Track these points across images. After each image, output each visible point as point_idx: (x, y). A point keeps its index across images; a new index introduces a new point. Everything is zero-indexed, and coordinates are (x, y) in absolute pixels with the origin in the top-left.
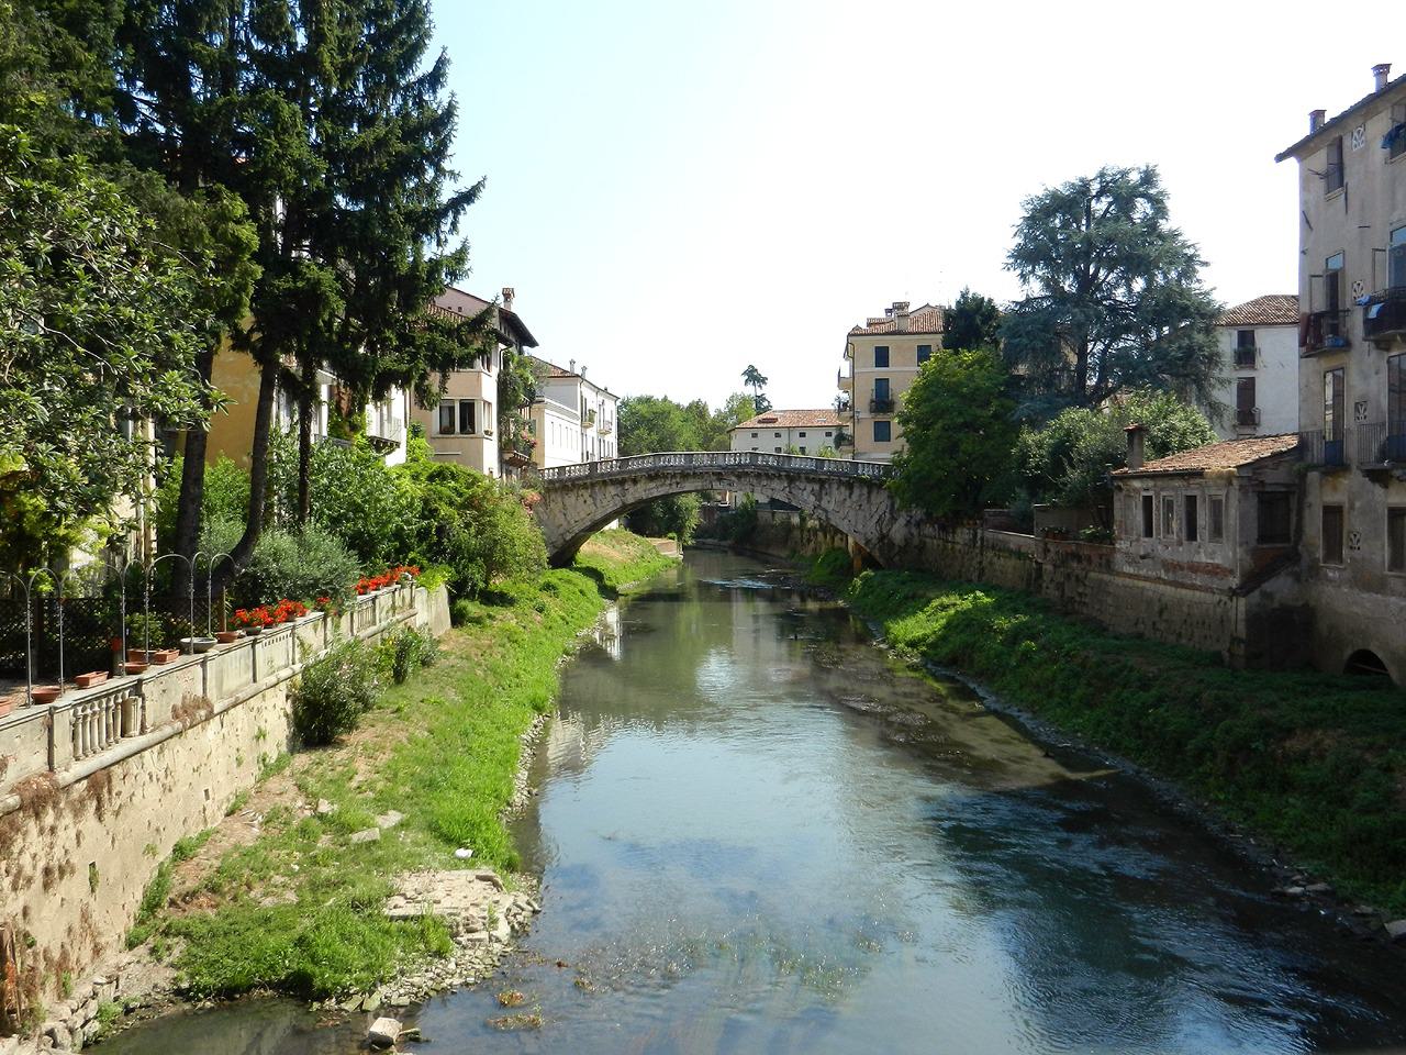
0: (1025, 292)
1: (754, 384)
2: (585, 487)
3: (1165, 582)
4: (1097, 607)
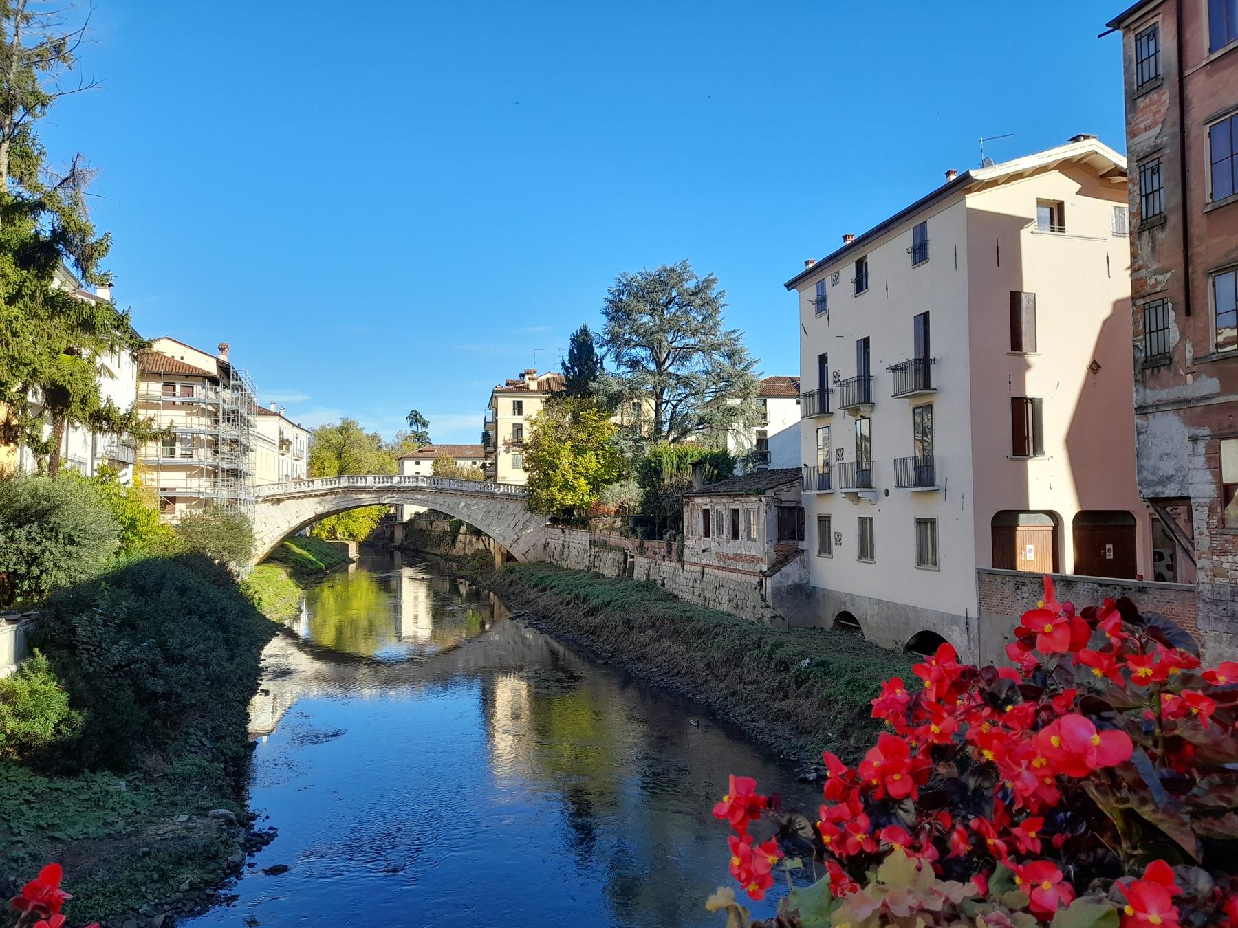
3: (718, 568)
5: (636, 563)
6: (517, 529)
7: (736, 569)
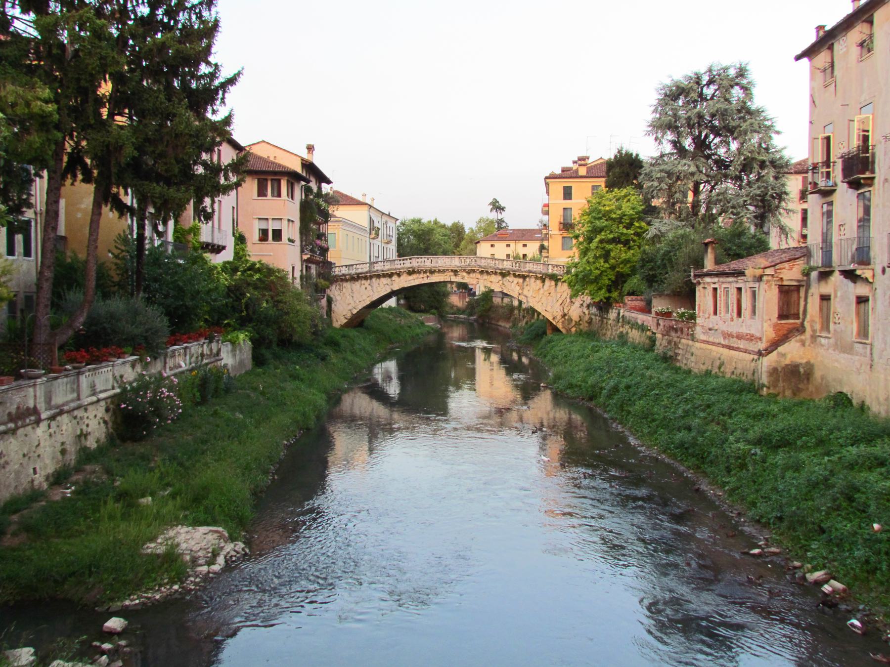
0: (660, 150)
1: (497, 211)
2: (366, 278)
3: (724, 346)
4: (685, 362)
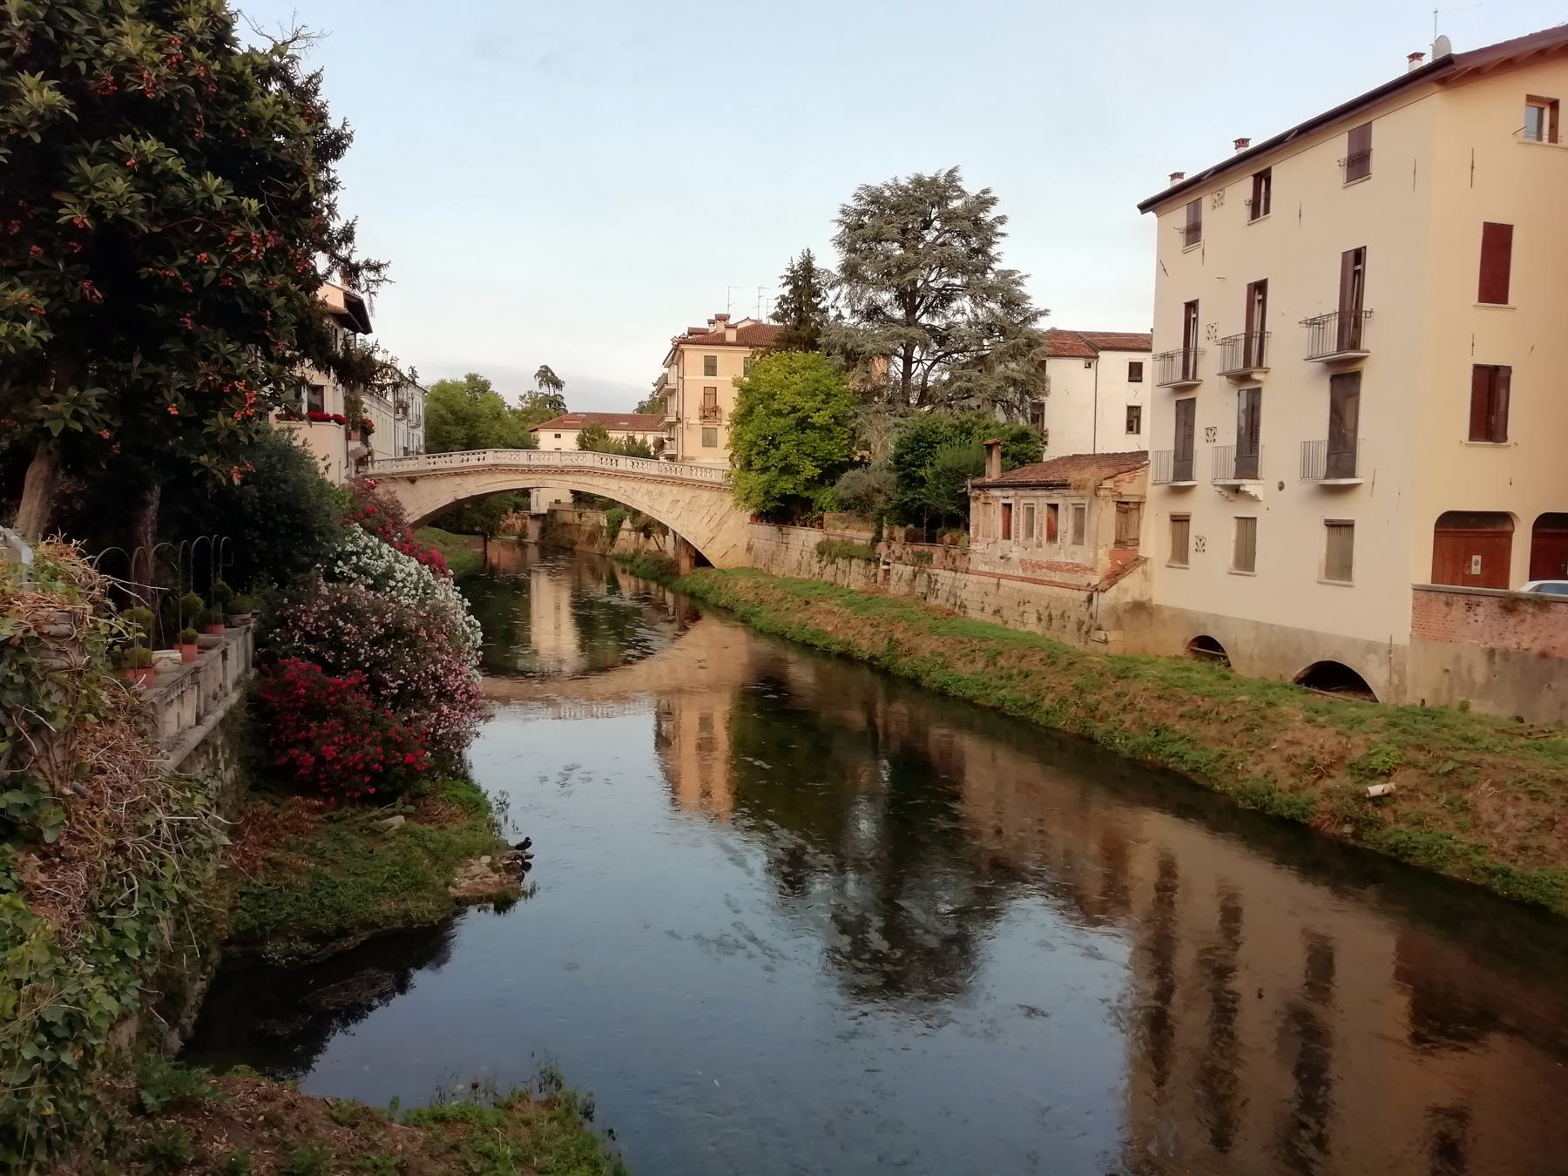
3: (1022, 579)
5: (893, 572)
6: (712, 525)
7: (1051, 582)
